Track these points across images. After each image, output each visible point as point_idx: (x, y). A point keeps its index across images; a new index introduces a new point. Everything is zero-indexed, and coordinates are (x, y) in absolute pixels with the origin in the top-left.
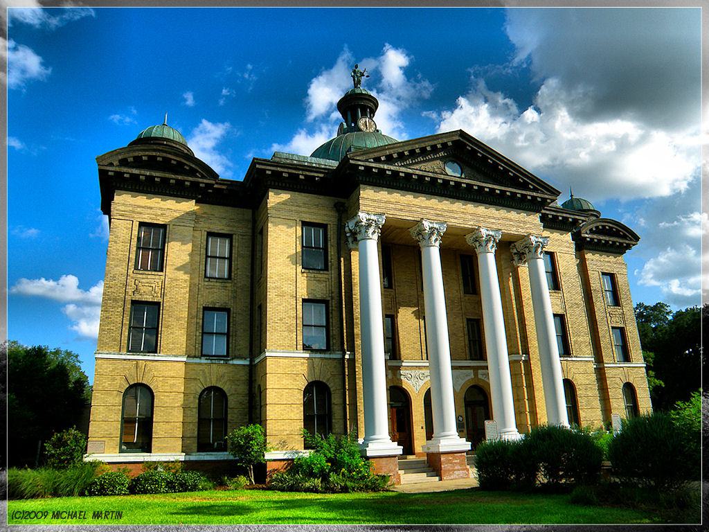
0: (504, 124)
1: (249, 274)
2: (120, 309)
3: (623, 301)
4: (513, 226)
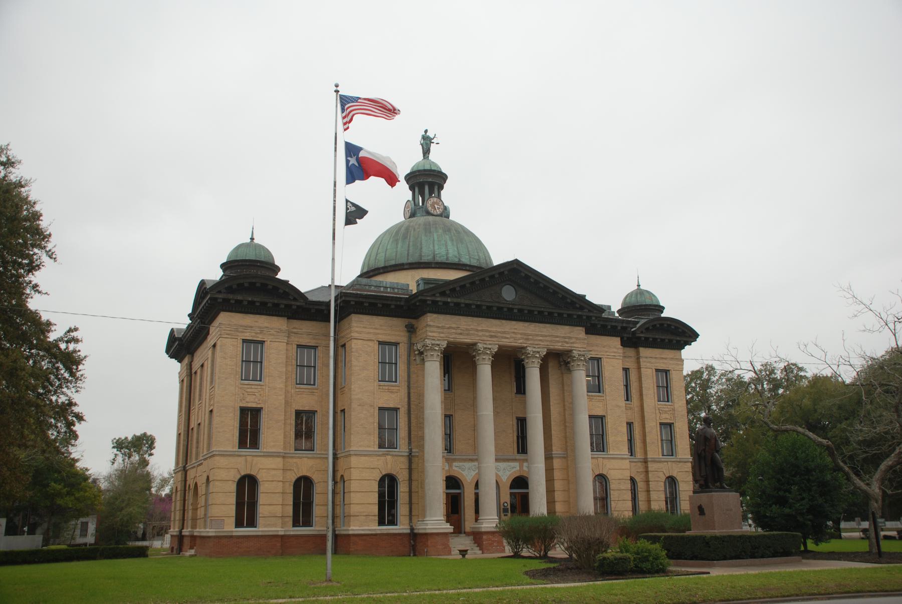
0: (333, 579)
4: (558, 342)
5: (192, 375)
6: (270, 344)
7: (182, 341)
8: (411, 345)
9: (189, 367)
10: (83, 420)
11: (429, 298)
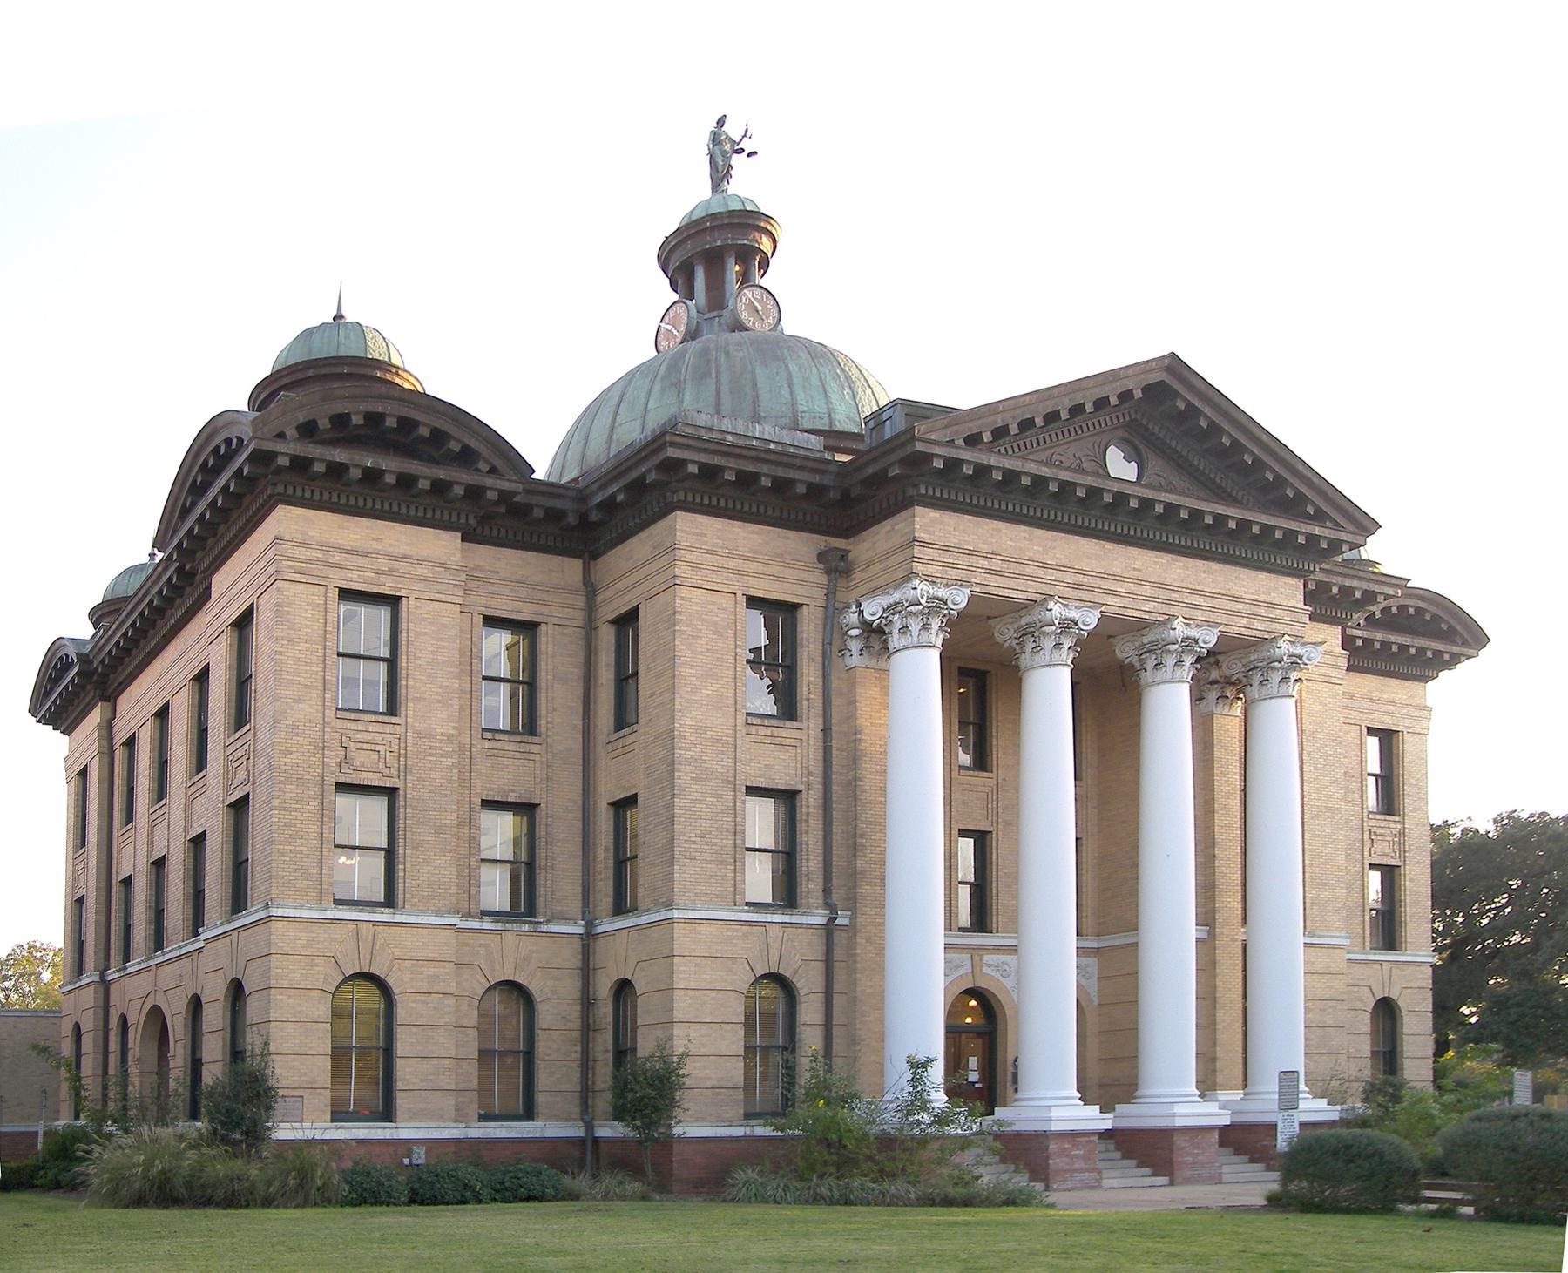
1: (579, 723)
2: (314, 805)
3: (1408, 802)
5: (112, 752)
6: (417, 607)
7: (91, 662)
8: (832, 611)
9: (105, 733)
10: (338, 317)
11: (937, 450)
